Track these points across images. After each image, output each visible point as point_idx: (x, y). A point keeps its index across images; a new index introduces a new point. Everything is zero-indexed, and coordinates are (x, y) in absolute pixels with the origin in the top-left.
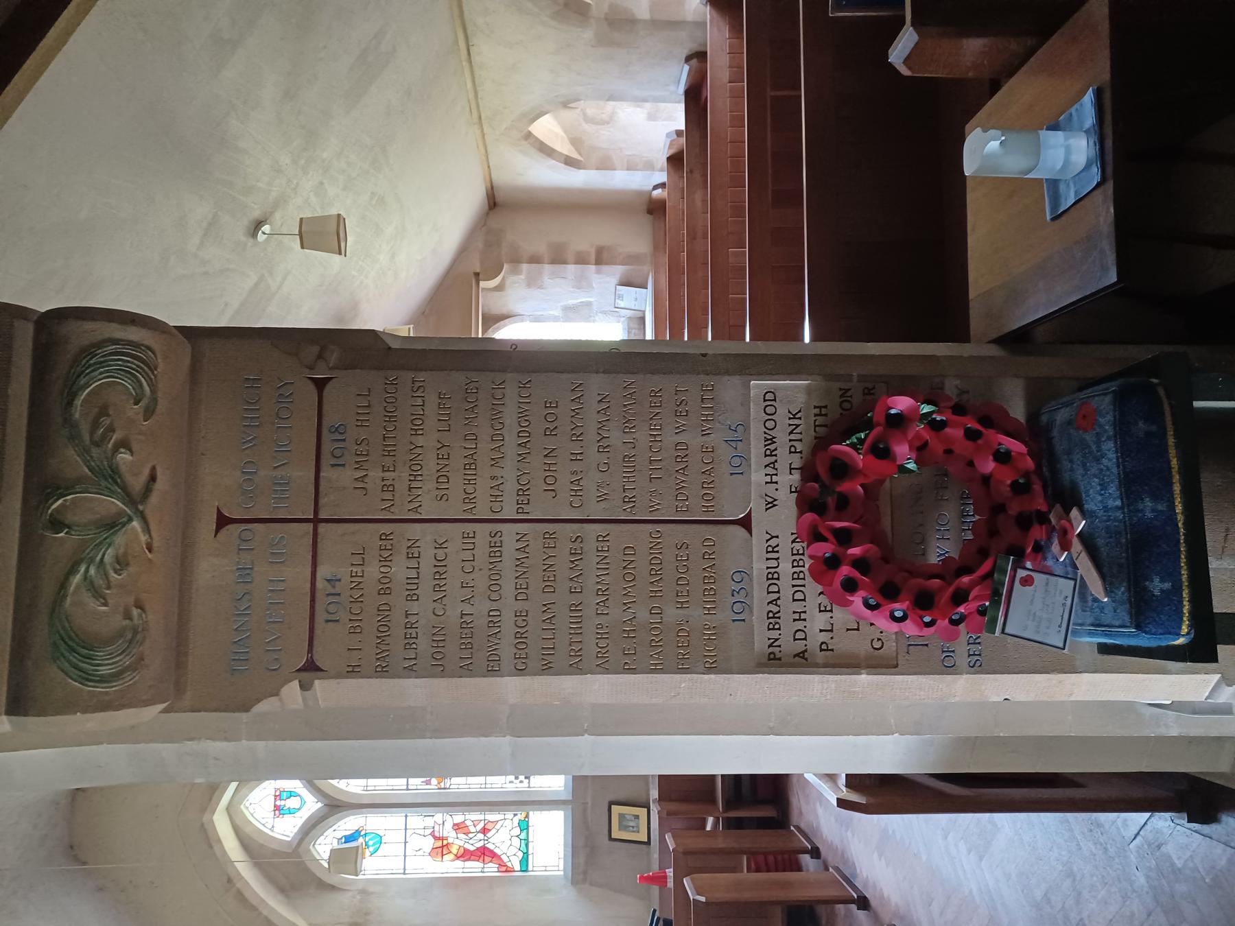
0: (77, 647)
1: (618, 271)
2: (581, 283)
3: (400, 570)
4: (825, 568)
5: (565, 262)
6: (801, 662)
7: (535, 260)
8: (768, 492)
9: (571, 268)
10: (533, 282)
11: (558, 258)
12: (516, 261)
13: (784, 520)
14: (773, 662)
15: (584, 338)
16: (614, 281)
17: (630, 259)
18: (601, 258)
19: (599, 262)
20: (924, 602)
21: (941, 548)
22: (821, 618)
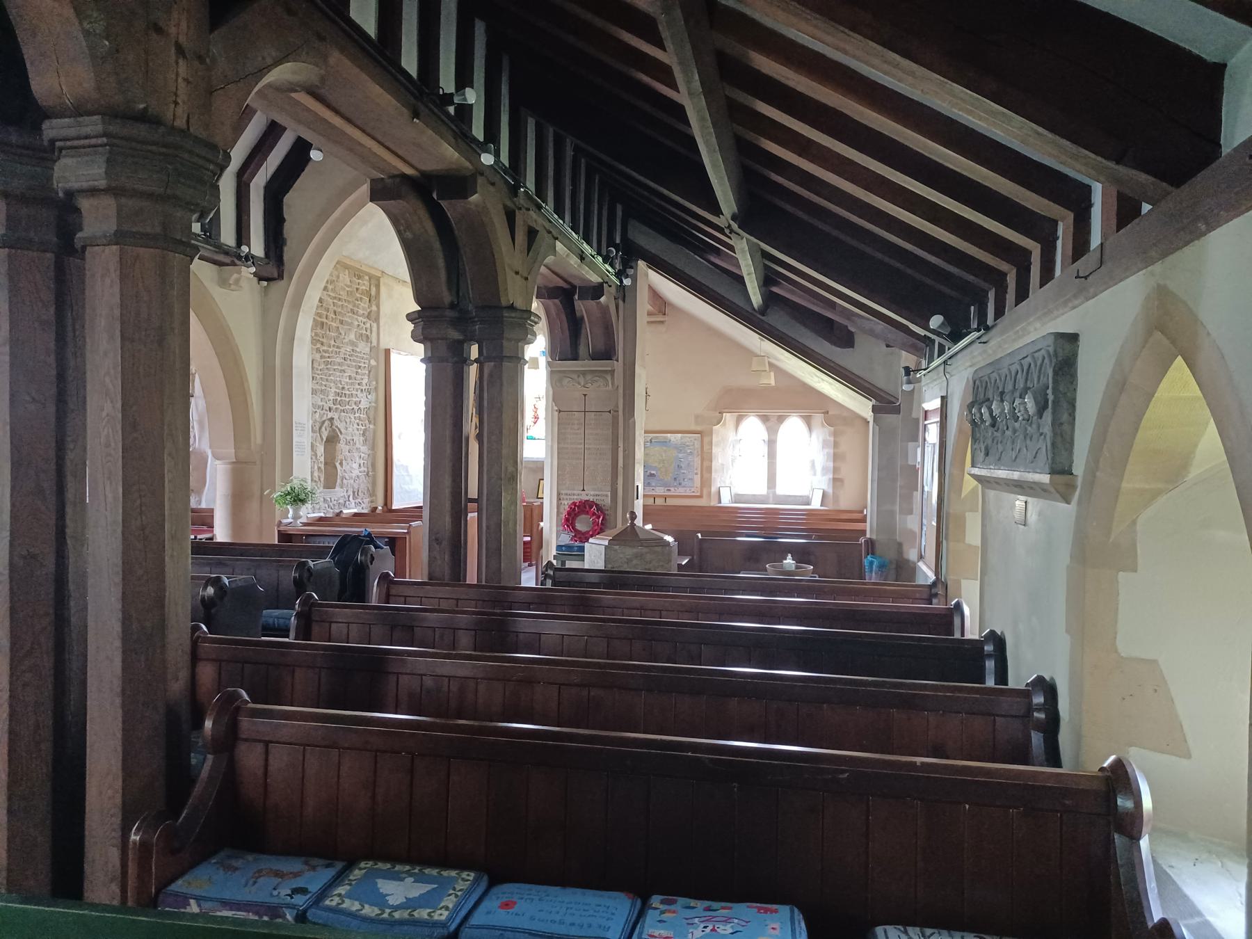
0: (560, 380)
1: (830, 491)
2: (825, 469)
3: (576, 427)
4: (574, 504)
5: (834, 461)
6: (559, 499)
7: (836, 445)
8: (588, 495)
9: (831, 464)
10: (825, 444)
11: (837, 457)
12: (835, 434)
13: (585, 498)
14: (559, 494)
15: (422, 463)
16: (825, 487)
17: (836, 498)
18: (837, 481)
19: (835, 480)
20: (567, 520)
21: (579, 526)
22: (566, 504)
